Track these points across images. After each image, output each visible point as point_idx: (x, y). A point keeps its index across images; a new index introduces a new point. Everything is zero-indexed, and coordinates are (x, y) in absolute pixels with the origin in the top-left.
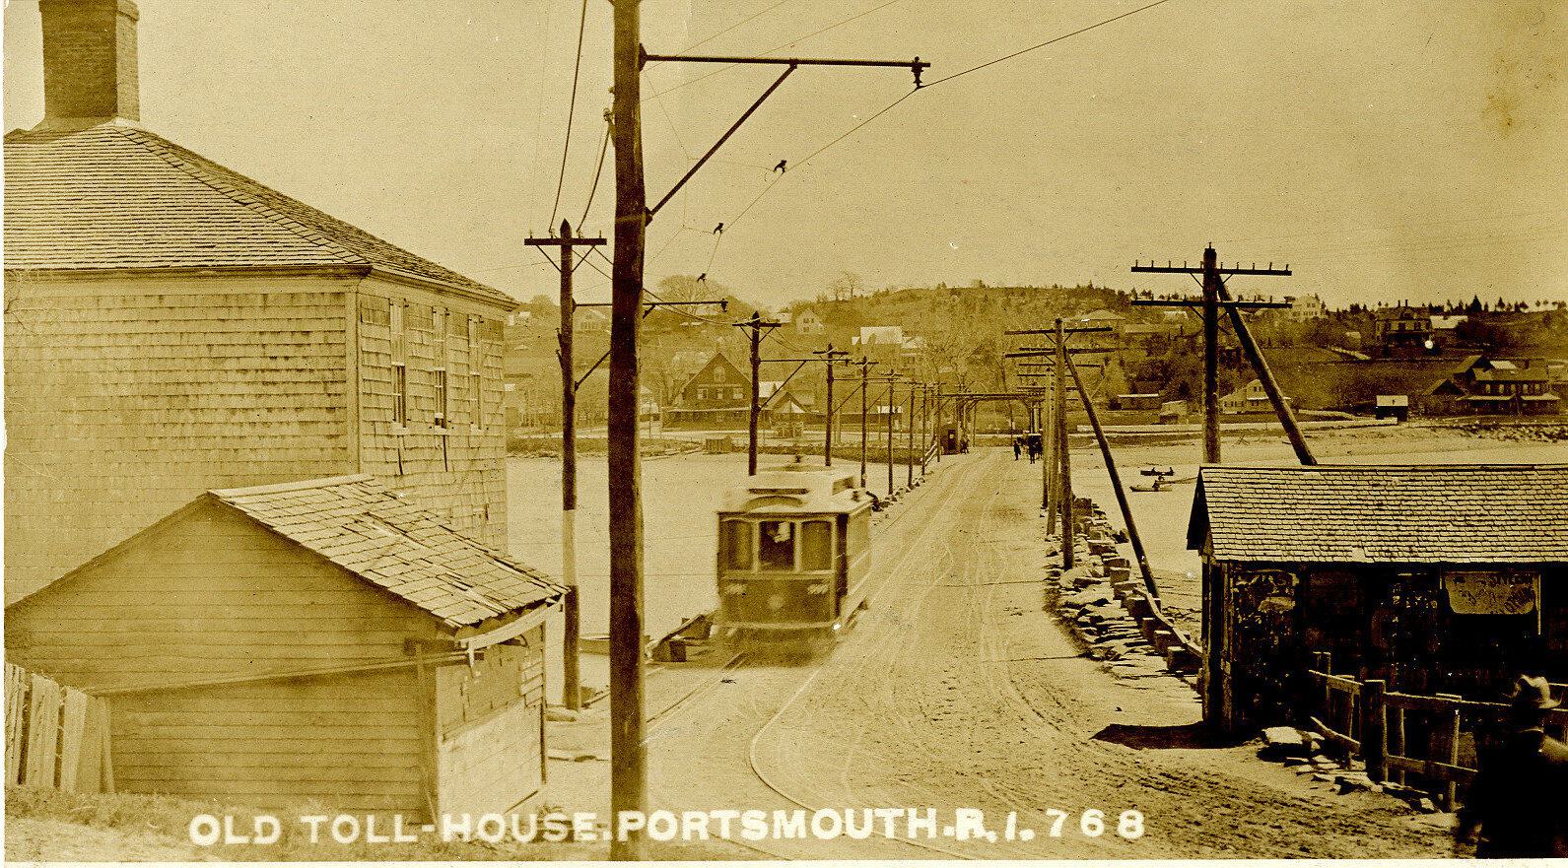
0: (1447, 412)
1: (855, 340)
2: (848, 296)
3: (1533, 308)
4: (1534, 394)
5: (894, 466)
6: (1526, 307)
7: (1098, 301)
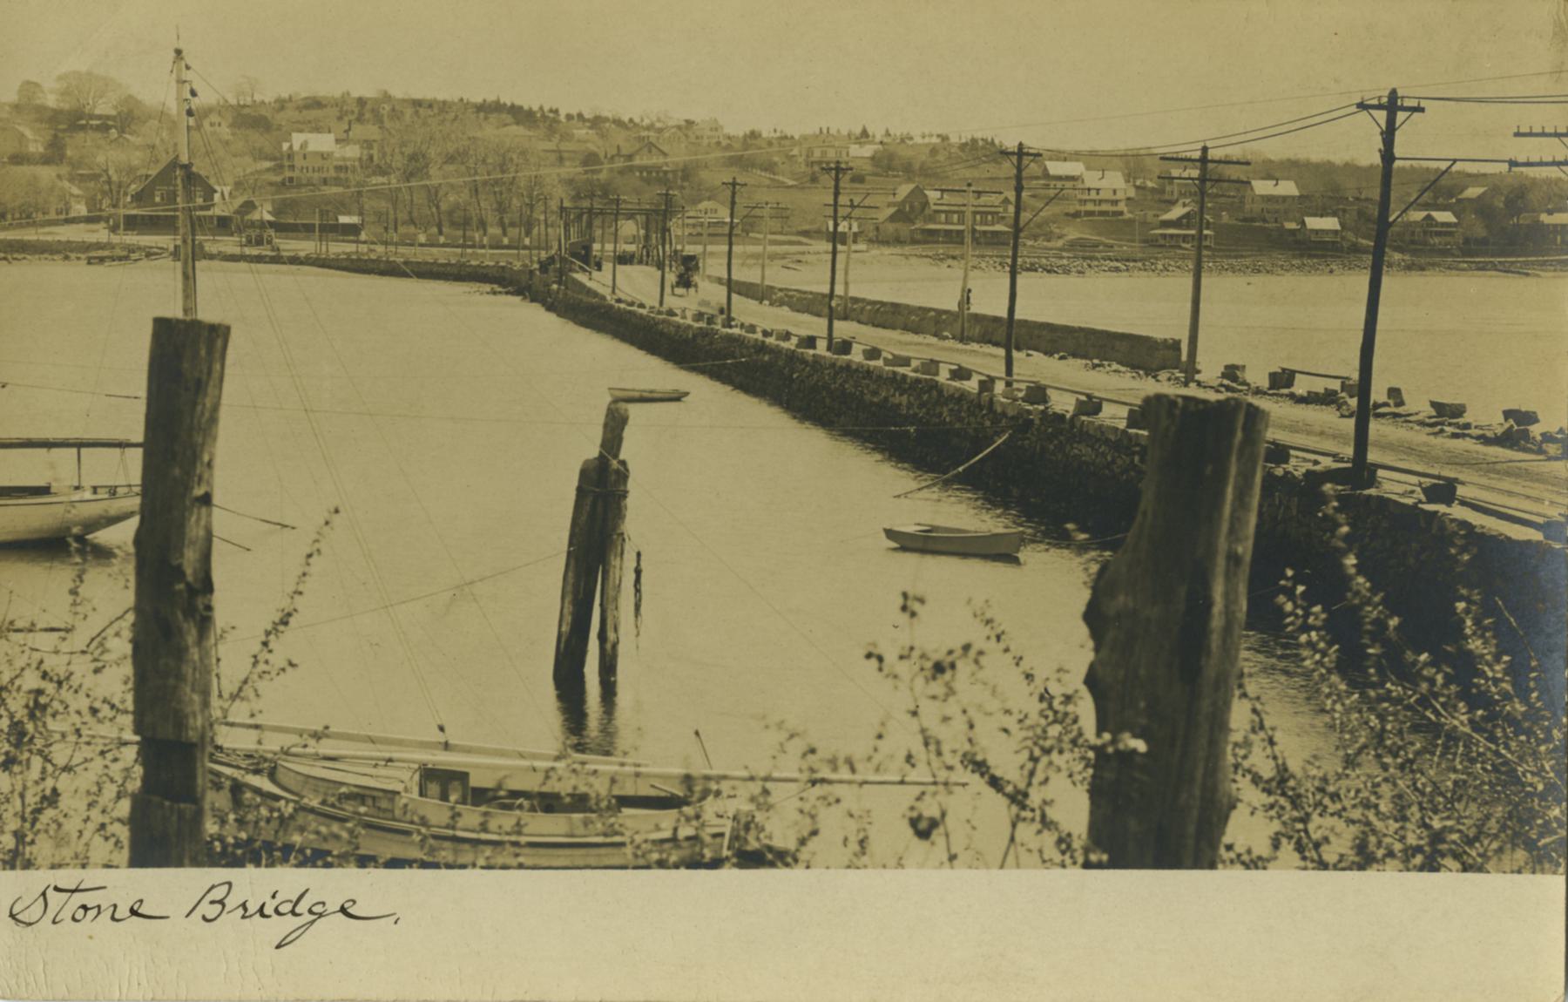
0: (898, 241)
1: (285, 146)
2: (249, 101)
3: (918, 140)
4: (986, 224)
5: (1004, 313)
6: (911, 138)
7: (508, 118)
